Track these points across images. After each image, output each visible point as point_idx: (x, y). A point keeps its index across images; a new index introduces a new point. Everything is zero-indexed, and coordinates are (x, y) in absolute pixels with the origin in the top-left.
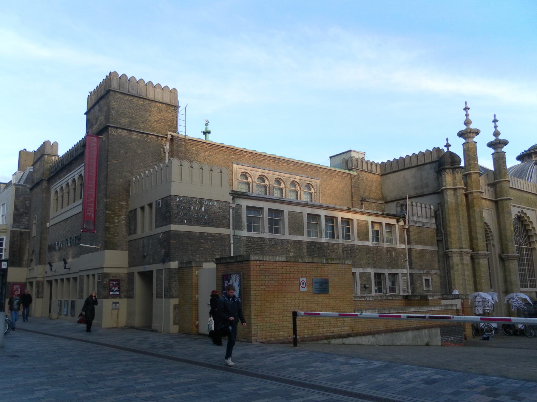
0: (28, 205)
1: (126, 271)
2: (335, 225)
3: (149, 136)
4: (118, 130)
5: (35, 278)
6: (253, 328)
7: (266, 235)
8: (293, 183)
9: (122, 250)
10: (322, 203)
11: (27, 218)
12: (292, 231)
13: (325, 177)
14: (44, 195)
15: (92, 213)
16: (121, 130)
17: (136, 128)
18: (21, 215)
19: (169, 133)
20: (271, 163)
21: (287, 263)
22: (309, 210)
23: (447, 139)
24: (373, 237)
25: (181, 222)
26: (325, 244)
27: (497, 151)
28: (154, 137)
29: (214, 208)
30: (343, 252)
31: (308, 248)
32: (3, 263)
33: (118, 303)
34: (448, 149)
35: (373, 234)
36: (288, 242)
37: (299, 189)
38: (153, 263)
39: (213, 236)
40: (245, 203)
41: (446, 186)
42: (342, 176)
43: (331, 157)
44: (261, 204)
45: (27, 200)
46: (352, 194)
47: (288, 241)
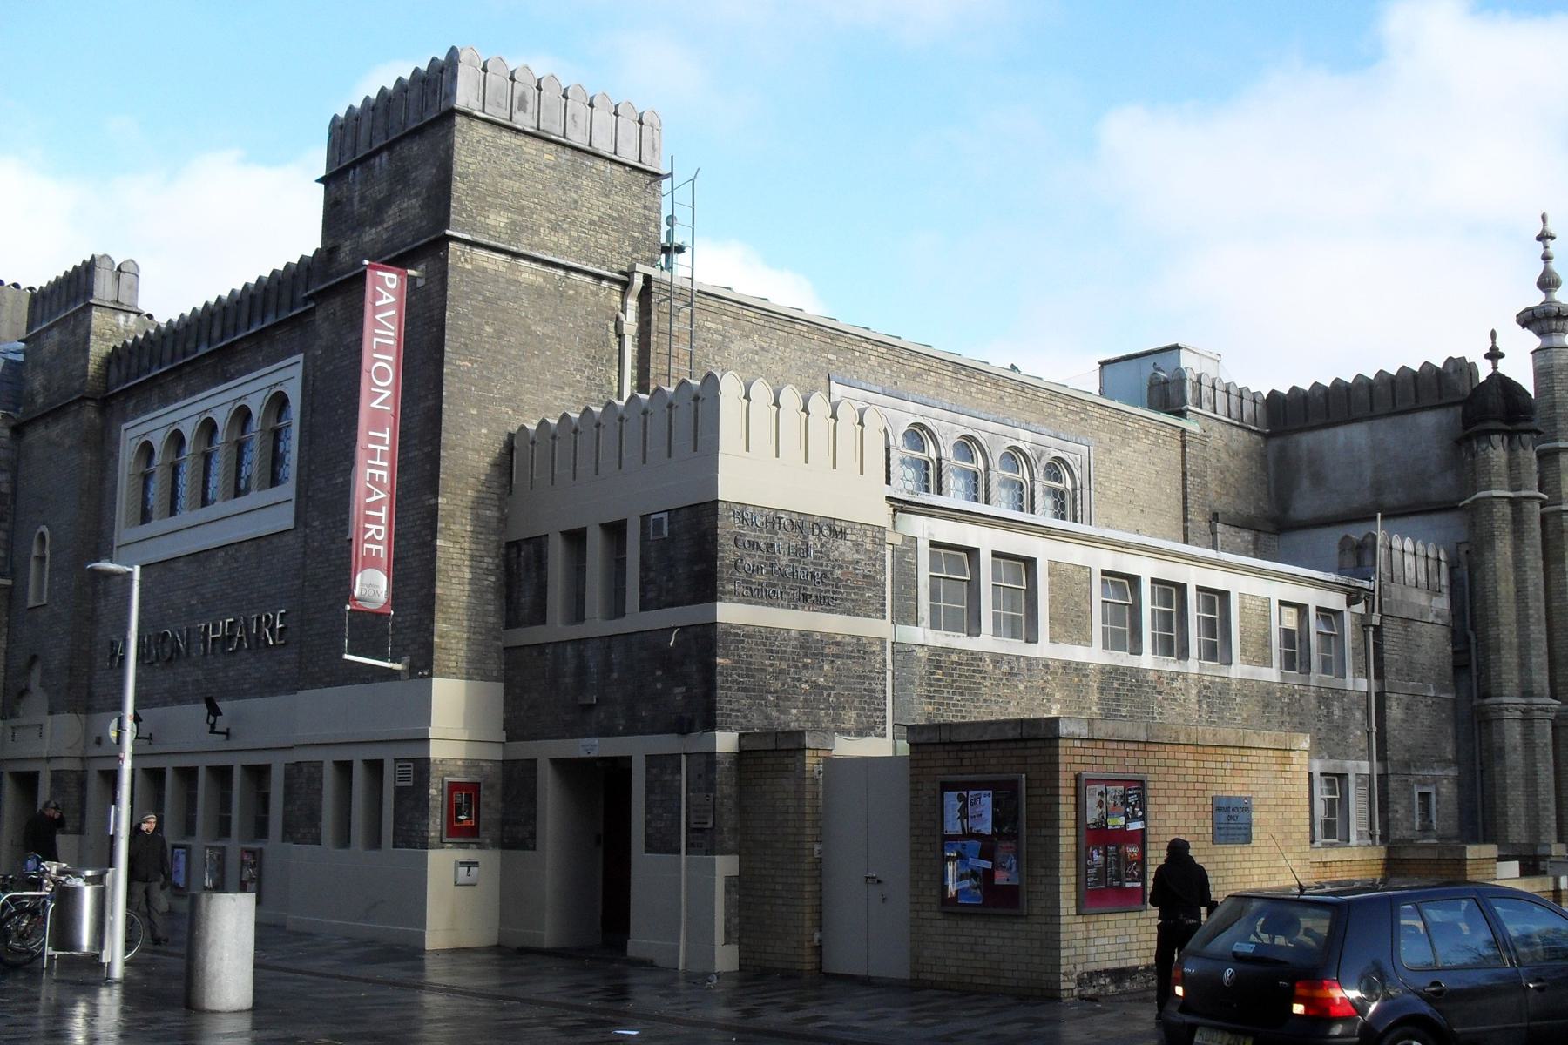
3: (574, 275)
4: (476, 251)
5: (48, 759)
6: (1063, 953)
8: (1014, 456)
12: (1057, 628)
13: (1105, 437)
14: (87, 456)
15: (379, 543)
16: (485, 253)
17: (532, 246)
21: (1149, 747)
23: (1493, 335)
27: (1547, 344)
28: (589, 279)
29: (842, 549)
30: (1199, 701)
31: (1102, 688)
33: (476, 864)
34: (1495, 368)
36: (1047, 666)
38: (628, 732)
39: (838, 644)
40: (924, 529)
41: (1489, 488)
42: (1157, 436)
43: (1103, 364)
46: (1185, 498)
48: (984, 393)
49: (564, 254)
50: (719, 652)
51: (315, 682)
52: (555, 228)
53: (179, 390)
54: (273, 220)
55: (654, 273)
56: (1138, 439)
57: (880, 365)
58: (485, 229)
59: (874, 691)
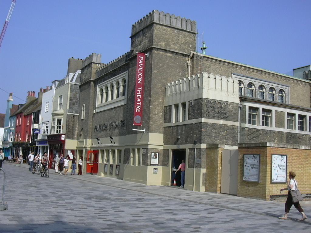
0: (78, 97)
1: (162, 148)
2: (304, 121)
7: (260, 127)
8: (272, 89)
9: (160, 133)
10: (296, 104)
11: (77, 106)
18: (74, 104)
19: (191, 52)
20: (257, 74)
22: (289, 111)
24: (299, 127)
25: (209, 117)
26: (298, 135)
29: (229, 108)
31: (287, 137)
32: (62, 136)
35: (299, 124)
36: (274, 132)
37: (265, 91)
38: (186, 143)
39: (228, 127)
40: (247, 105)
43: (294, 70)
44: (293, 111)
45: (77, 94)
47: (274, 132)
48: (265, 76)
49: (176, 50)
50: (202, 128)
51: (129, 133)
52: (174, 44)
53: (107, 78)
54: (121, 47)
55: (195, 53)
56: (300, 85)
57: (243, 71)
58: (160, 45)
59: (235, 136)
